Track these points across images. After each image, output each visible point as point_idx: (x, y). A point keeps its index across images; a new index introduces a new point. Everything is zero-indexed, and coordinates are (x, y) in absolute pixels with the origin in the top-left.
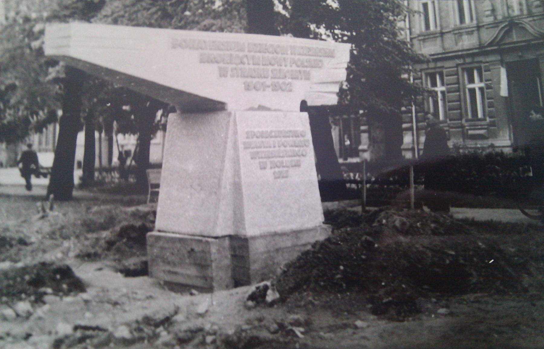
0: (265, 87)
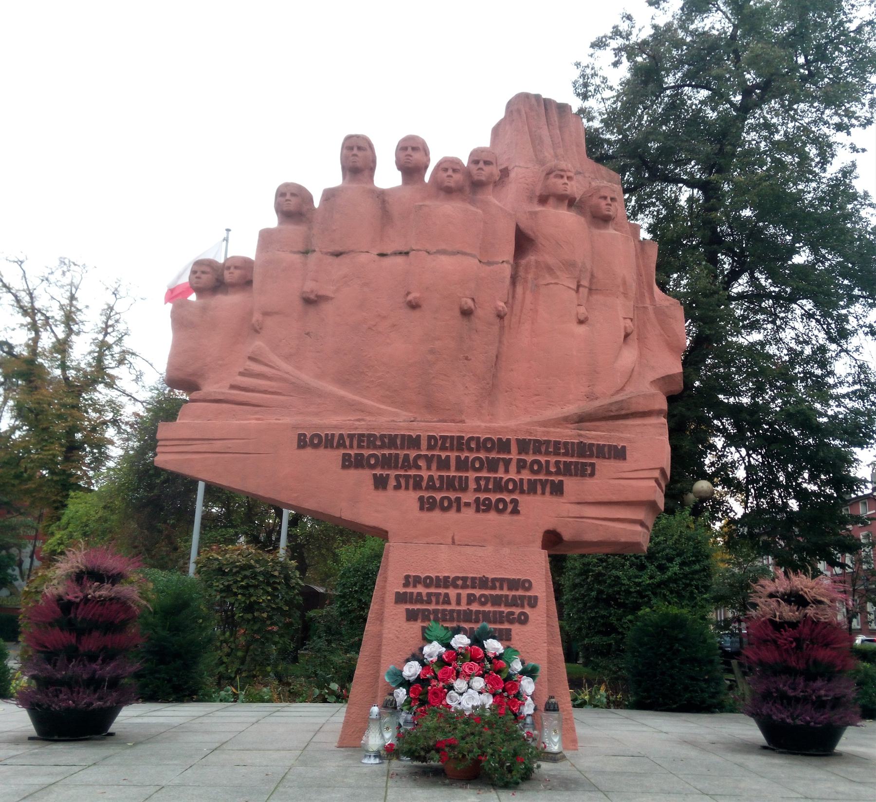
0: (458, 505)
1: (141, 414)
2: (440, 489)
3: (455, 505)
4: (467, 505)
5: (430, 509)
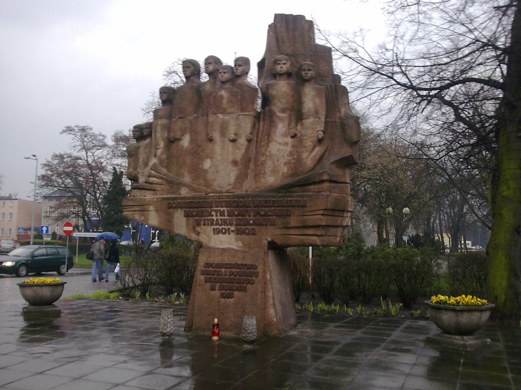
1: (43, 184)
2: (221, 225)
3: (228, 232)
4: (233, 231)
5: (218, 233)
